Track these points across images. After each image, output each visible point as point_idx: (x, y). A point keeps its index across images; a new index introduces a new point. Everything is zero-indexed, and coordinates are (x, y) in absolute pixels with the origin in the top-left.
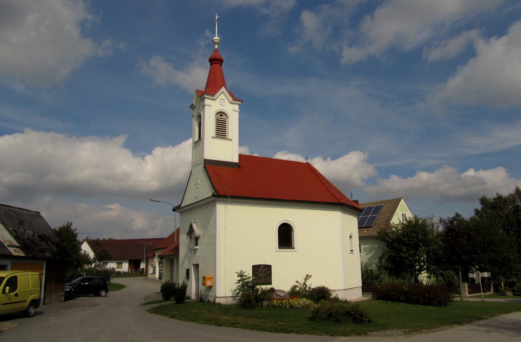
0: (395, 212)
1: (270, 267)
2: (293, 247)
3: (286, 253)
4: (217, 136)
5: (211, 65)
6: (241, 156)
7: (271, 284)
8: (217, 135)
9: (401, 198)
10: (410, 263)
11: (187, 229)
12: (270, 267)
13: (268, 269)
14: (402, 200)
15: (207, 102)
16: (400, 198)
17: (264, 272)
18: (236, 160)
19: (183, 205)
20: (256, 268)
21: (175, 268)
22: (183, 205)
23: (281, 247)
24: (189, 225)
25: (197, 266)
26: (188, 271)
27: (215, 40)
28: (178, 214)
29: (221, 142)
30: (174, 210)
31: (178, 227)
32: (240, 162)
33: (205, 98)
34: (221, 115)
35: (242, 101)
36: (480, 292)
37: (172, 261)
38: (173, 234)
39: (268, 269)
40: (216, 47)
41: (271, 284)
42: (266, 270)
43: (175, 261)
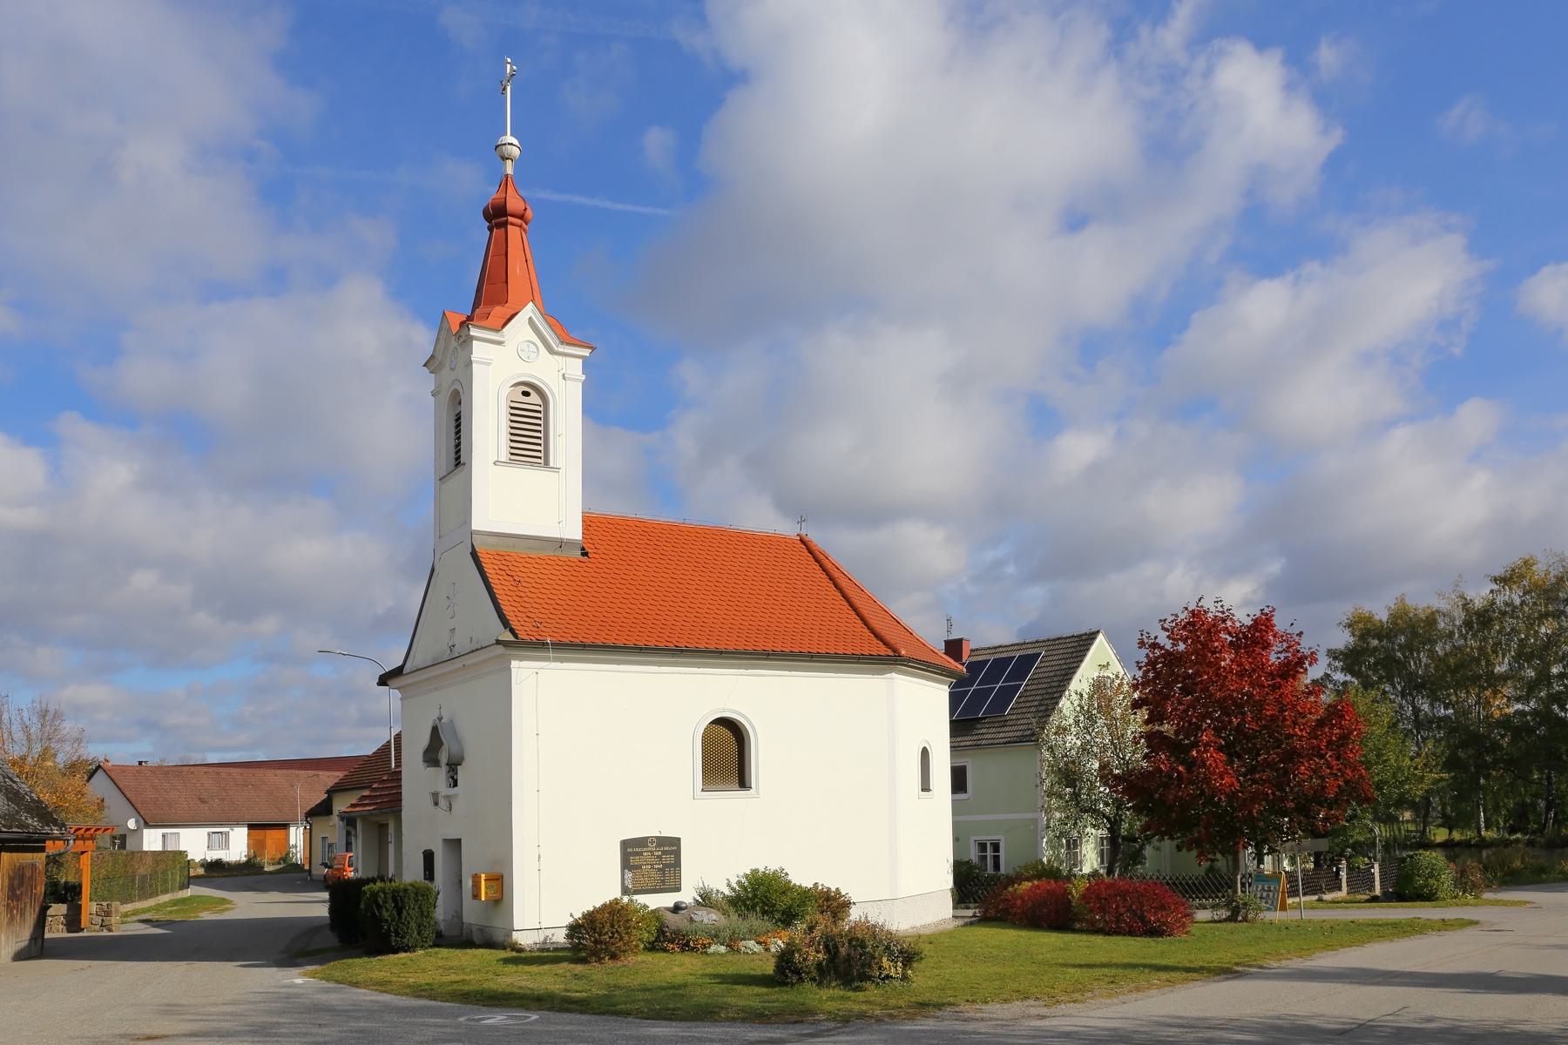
0: (1074, 673)
1: (676, 842)
2: (747, 785)
3: (729, 801)
4: (510, 460)
5: (490, 229)
6: (589, 523)
7: (678, 889)
8: (512, 454)
9: (1098, 632)
10: (1525, 720)
11: (424, 740)
12: (676, 842)
13: (670, 848)
14: (1100, 637)
15: (479, 350)
16: (1094, 630)
17: (658, 857)
18: (574, 532)
19: (417, 660)
20: (631, 851)
21: (391, 848)
22: (407, 669)
23: (710, 788)
24: (429, 730)
25: (455, 845)
26: (429, 857)
27: (510, 147)
28: (396, 694)
29: (527, 477)
30: (384, 680)
31: (397, 732)
32: (587, 536)
33: (472, 338)
34: (526, 394)
35: (593, 349)
36: (1298, 895)
37: (382, 828)
38: (385, 749)
39: (670, 848)
40: (509, 168)
41: (678, 889)
42: (664, 853)
43: (391, 829)
